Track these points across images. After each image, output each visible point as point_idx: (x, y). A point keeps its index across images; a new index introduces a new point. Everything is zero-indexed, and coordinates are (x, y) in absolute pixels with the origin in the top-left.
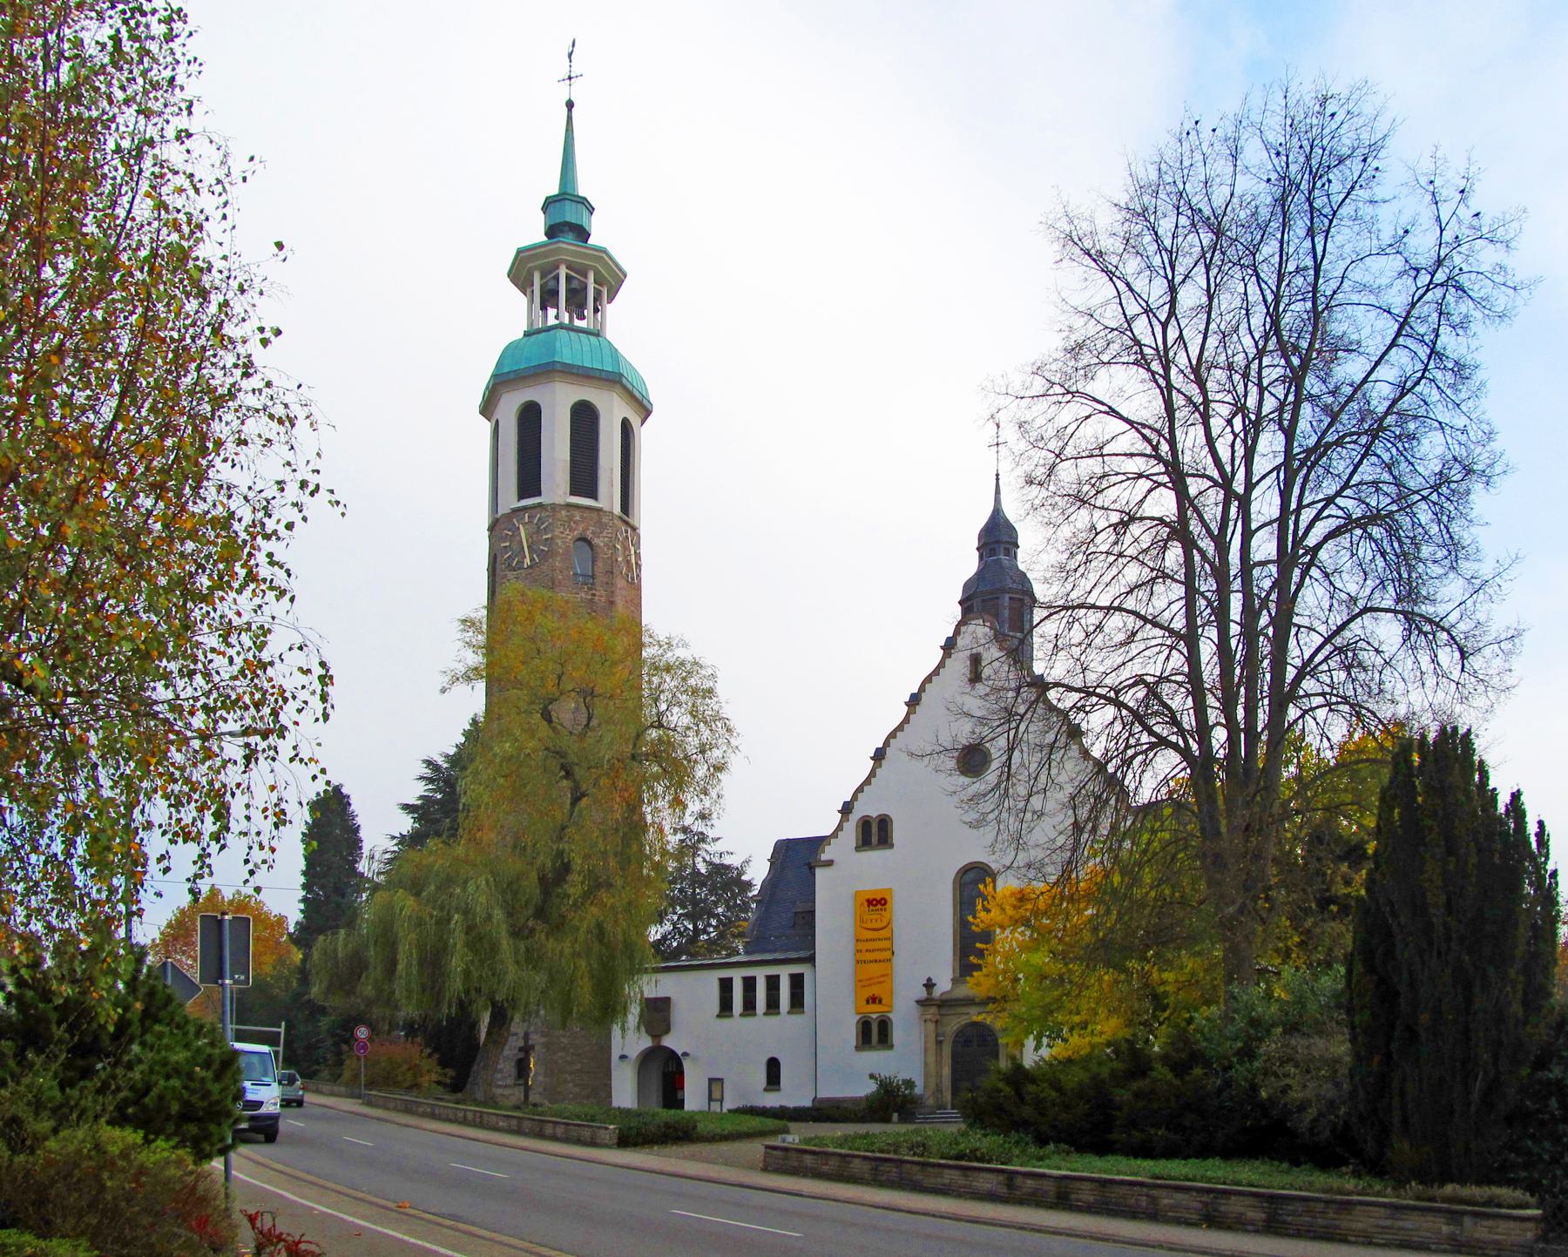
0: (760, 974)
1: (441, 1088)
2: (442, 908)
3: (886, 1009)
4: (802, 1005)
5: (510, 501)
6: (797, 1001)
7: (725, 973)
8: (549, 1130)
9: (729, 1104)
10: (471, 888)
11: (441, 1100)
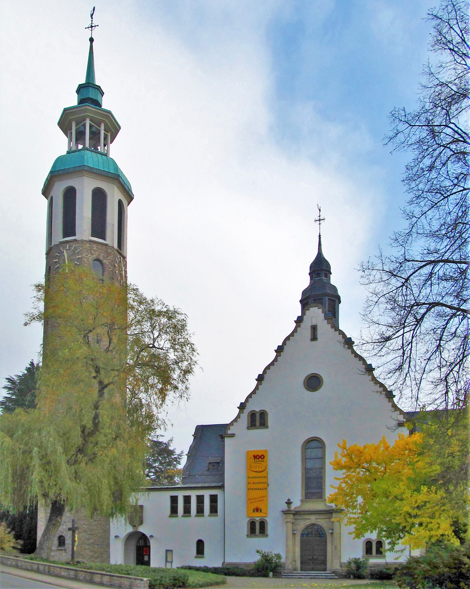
0: (193, 494)
1: (15, 551)
2: (26, 444)
3: (264, 515)
4: (216, 512)
5: (58, 237)
6: (214, 510)
7: (174, 493)
8: (97, 578)
9: (175, 565)
10: (44, 433)
11: (17, 557)
